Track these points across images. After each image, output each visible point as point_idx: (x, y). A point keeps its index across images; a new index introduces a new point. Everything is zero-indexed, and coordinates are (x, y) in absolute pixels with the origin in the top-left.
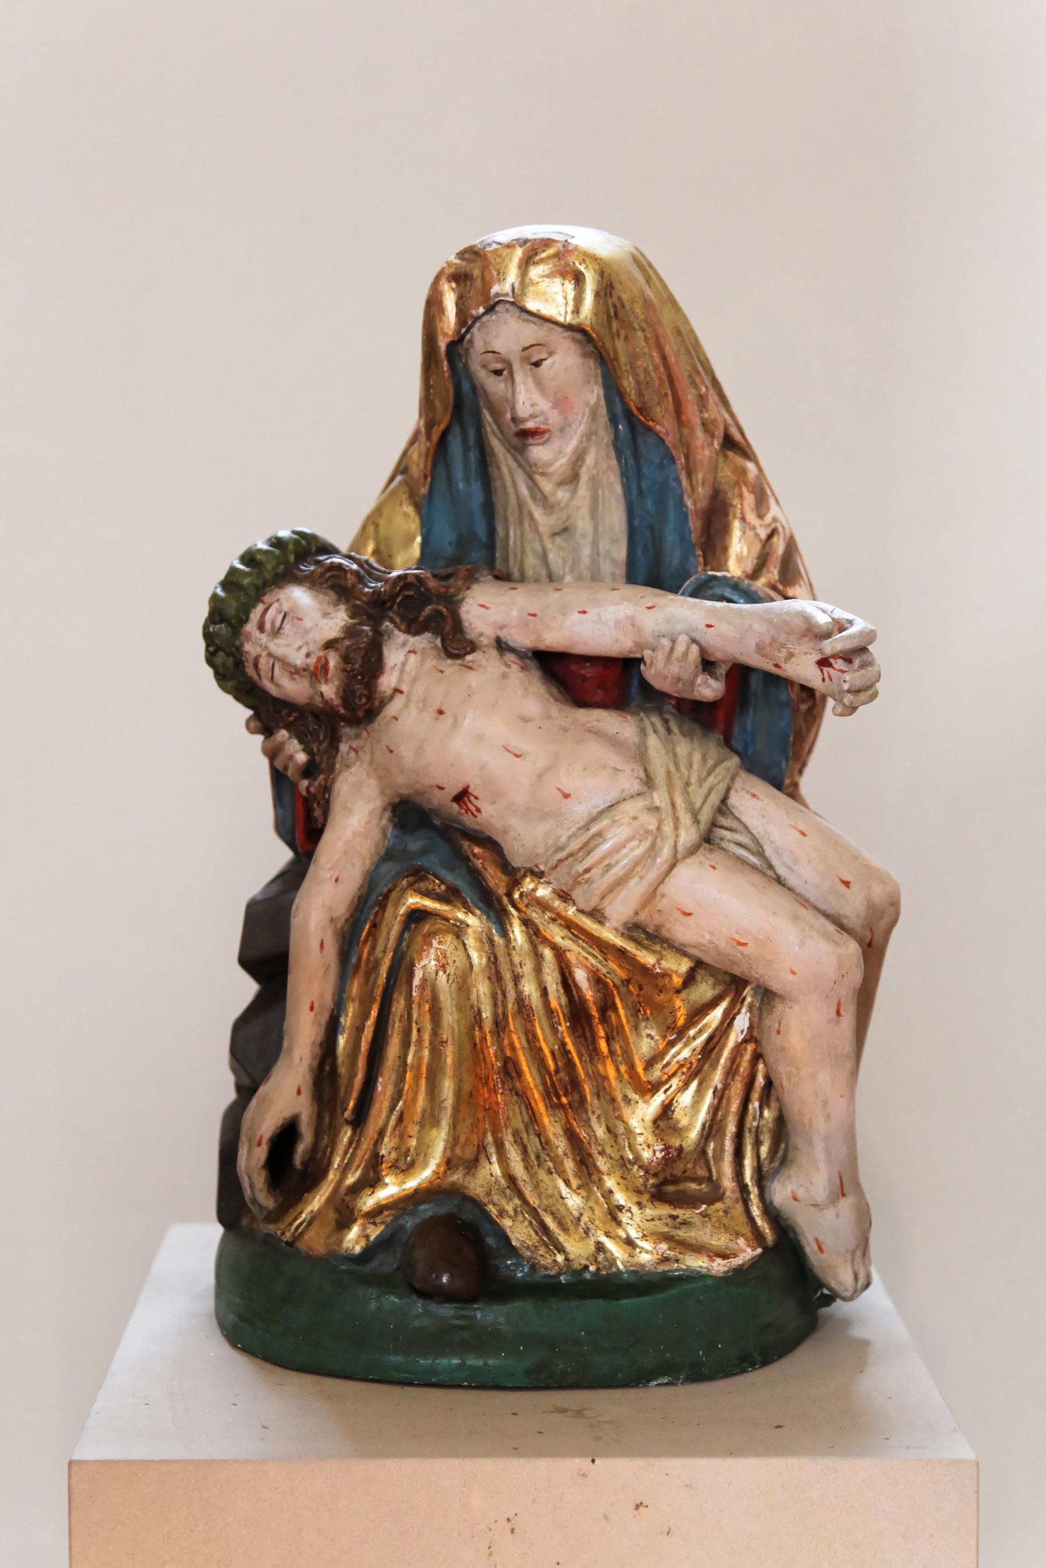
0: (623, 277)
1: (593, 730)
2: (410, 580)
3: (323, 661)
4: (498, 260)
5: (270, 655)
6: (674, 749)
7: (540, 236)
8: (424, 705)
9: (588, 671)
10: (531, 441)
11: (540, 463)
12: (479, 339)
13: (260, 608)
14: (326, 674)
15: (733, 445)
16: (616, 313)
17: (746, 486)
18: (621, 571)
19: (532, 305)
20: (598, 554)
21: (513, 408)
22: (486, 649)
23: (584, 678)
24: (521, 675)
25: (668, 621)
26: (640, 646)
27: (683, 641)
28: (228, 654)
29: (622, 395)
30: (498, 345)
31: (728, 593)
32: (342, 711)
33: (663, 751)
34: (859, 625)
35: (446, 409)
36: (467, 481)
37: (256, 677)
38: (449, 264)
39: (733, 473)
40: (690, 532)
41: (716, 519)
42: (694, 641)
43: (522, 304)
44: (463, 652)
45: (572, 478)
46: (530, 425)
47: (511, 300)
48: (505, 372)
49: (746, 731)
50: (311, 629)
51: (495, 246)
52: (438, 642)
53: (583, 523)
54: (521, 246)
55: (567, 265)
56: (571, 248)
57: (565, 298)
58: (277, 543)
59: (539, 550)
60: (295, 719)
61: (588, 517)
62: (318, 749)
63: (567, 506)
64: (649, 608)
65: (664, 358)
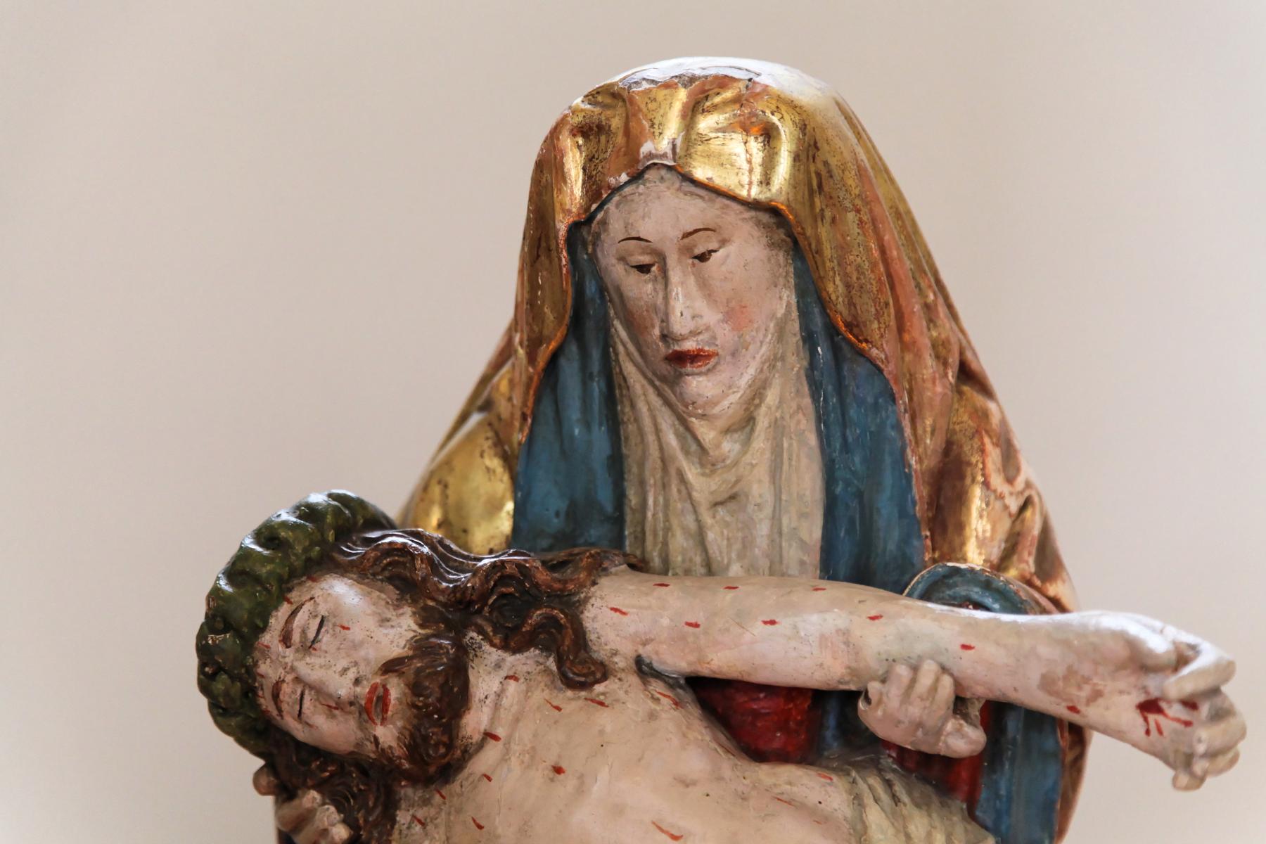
0: (830, 133)
1: (784, 797)
2: (509, 570)
3: (380, 690)
4: (652, 106)
5: (298, 680)
6: (905, 827)
7: (713, 72)
8: (532, 758)
9: (762, 704)
10: (689, 368)
11: (700, 401)
12: (616, 219)
13: (284, 610)
14: (385, 709)
15: (969, 376)
16: (820, 186)
17: (990, 437)
18: (814, 558)
19: (701, 172)
20: (780, 533)
21: (665, 320)
22: (623, 675)
23: (756, 715)
24: (676, 713)
25: (901, 638)
26: (854, 672)
27: (929, 671)
28: (233, 678)
29: (824, 304)
30: (646, 229)
31: (976, 593)
32: (407, 766)
33: (891, 831)
34: (1208, 657)
35: (559, 319)
36: (587, 425)
37: (275, 713)
38: (575, 112)
39: (971, 417)
40: (914, 503)
41: (949, 481)
42: (944, 669)
43: (687, 169)
44: (591, 679)
45: (745, 422)
46: (689, 345)
47: (671, 163)
48: (654, 269)
49: (998, 796)
50: (362, 643)
51: (645, 85)
52: (551, 663)
53: (759, 489)
54: (685, 86)
55: (754, 114)
56: (758, 90)
57: (749, 162)
58: (309, 513)
59: (692, 526)
60: (332, 776)
61: (766, 480)
62: (366, 821)
63: (736, 463)
64: (873, 618)
65: (883, 251)
